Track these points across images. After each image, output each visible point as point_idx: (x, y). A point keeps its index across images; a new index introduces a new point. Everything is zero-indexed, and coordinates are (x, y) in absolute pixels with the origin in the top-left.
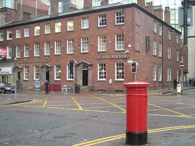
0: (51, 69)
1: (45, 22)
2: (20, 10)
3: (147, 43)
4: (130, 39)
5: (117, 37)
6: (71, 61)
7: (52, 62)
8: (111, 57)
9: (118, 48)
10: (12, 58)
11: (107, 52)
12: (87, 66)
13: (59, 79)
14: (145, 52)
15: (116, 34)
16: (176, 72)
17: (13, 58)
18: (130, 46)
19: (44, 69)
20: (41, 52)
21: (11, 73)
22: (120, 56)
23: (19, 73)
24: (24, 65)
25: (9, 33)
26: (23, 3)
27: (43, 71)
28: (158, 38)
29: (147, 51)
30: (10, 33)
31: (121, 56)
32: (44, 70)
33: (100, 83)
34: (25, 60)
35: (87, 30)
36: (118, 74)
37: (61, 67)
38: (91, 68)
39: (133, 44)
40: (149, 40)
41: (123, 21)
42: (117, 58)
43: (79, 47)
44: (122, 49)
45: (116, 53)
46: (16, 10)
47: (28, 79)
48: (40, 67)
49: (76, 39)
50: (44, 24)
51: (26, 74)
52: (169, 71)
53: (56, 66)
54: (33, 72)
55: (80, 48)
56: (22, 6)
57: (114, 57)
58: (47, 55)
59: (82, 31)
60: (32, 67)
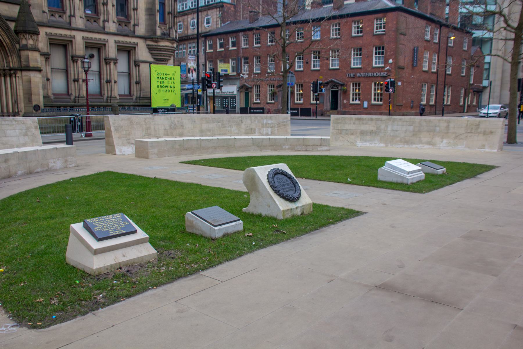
4: (392, 53)
5: (376, 49)
14: (410, 67)
16: (459, 92)
21: (235, 93)
22: (378, 74)
30: (232, 40)
31: (380, 74)
33: (353, 106)
36: (375, 95)
43: (327, 61)
45: (373, 70)
48: (275, 86)
52: (448, 91)
54: (267, 93)
55: (328, 62)
60: (265, 85)
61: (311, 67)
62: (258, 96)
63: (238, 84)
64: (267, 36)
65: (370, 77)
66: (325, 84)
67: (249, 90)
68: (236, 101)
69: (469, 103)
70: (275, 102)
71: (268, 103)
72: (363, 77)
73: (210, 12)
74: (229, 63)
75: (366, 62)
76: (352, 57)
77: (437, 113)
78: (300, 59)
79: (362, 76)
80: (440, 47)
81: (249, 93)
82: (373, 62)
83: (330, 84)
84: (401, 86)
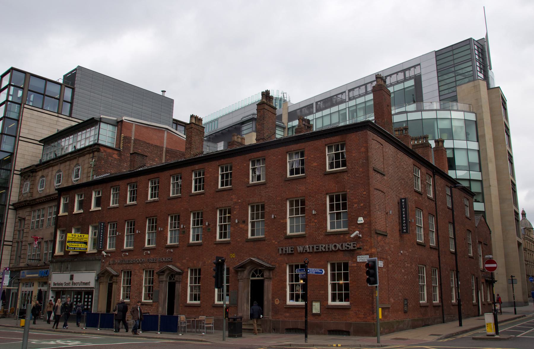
0: (181, 276)
1: (172, 172)
3: (402, 214)
4: (362, 205)
5: (331, 200)
6: (218, 258)
7: (184, 261)
8: (317, 249)
11: (307, 235)
13: (198, 302)
14: (397, 234)
15: (327, 194)
19: (164, 278)
20: (161, 237)
21: (92, 285)
23: (110, 286)
25: (96, 195)
27: (162, 281)
28: (427, 204)
29: (403, 232)
31: (342, 245)
32: (164, 279)
34: (126, 255)
35: (262, 187)
36: (334, 289)
37: (202, 273)
38: (270, 275)
40: (405, 207)
41: (344, 164)
42: (331, 250)
43: (243, 226)
47: (129, 301)
48: (155, 272)
49: (236, 207)
53: (192, 270)
54: (141, 285)
57: (325, 248)
61: (216, 237)
62: (127, 289)
63: (98, 268)
64: (148, 187)
65: (322, 251)
66: (239, 268)
67: (114, 278)
68: (92, 298)
69: (483, 300)
70: (153, 302)
71: (143, 304)
72: (309, 253)
73: (81, 159)
74: (88, 234)
75: (314, 224)
76: (288, 216)
77: (445, 319)
78: (198, 225)
79: (308, 251)
80: (437, 207)
81: (114, 285)
82: (326, 223)
83: (248, 268)
84: (384, 270)
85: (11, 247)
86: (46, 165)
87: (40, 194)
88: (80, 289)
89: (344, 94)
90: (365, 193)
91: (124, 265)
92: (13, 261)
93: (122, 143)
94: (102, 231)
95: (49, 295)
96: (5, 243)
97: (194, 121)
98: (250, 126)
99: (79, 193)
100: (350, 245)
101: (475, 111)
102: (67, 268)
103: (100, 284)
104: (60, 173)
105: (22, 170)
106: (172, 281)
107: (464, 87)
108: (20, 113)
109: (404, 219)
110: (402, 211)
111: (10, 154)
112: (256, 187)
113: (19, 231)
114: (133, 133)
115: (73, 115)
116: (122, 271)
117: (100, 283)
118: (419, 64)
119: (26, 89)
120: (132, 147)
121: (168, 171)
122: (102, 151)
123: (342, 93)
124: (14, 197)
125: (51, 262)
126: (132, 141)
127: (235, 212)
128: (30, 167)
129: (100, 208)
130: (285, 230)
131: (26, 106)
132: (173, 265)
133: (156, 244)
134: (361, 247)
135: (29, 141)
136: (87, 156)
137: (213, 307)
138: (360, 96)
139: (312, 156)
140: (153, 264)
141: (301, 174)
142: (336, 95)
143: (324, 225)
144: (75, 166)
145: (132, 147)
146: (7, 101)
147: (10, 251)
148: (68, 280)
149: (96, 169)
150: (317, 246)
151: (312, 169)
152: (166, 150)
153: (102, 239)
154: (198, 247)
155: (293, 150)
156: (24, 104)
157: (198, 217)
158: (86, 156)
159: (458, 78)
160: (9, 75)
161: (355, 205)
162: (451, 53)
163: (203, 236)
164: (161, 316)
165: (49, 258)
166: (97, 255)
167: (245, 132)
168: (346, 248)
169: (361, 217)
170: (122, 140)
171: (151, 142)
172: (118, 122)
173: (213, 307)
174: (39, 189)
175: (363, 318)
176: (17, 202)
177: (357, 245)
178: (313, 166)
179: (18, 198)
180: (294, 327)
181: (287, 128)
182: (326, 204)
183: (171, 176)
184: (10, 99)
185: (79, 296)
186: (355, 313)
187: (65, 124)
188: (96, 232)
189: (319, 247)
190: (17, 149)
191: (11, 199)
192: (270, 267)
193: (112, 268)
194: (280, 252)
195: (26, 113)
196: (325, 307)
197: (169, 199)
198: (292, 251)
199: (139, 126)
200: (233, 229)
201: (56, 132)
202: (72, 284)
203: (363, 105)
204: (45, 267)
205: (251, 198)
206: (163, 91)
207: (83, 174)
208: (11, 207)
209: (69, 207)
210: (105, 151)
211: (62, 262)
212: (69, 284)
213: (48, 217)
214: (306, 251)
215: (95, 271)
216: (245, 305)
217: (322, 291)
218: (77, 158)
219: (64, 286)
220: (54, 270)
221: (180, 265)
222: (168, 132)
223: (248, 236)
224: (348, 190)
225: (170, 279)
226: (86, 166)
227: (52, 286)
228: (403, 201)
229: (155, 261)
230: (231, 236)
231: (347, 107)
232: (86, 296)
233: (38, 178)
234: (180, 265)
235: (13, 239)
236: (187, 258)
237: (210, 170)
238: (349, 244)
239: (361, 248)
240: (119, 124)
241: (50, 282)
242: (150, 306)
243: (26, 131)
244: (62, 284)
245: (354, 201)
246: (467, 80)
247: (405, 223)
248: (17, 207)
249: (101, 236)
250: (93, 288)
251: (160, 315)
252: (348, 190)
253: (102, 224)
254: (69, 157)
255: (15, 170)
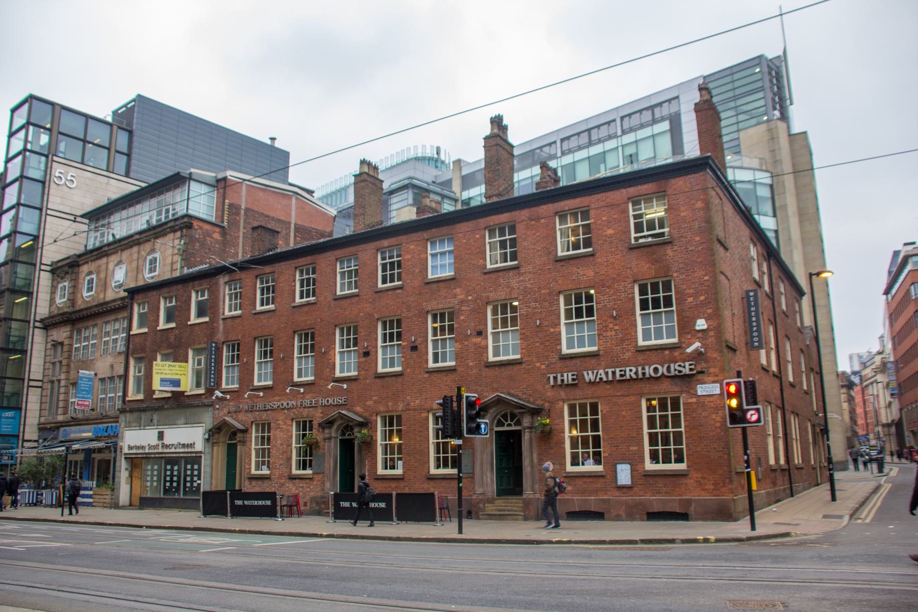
1: (338, 253)
2: (238, 227)
3: (750, 317)
4: (702, 298)
5: (643, 291)
7: (369, 403)
9: (570, 345)
10: (206, 389)
11: (601, 352)
12: (513, 416)
15: (635, 281)
17: (210, 391)
18: (701, 324)
19: (333, 432)
21: (199, 447)
24: (250, 417)
25: (197, 297)
26: (246, 204)
31: (668, 369)
33: (579, 482)
39: (715, 316)
42: (647, 376)
44: (587, 349)
45: (640, 358)
46: (223, 227)
48: (315, 424)
49: (463, 308)
50: (333, 258)
51: (262, 453)
54: (290, 445)
56: (246, 214)
58: (346, 374)
59: (491, 275)
60: (285, 423)
63: (208, 419)
65: (631, 379)
67: (239, 435)
68: (199, 470)
70: (314, 474)
71: (293, 478)
72: (606, 382)
74: (187, 362)
75: (614, 333)
78: (348, 346)
79: (605, 379)
83: (491, 411)
85: (40, 389)
86: (96, 253)
87: (88, 302)
88: (178, 455)
89: (553, 146)
90: (706, 278)
91: (257, 413)
92: (46, 413)
93: (226, 215)
94: (213, 357)
95: (121, 467)
96: (32, 383)
97: (366, 169)
98: (405, 196)
99: (197, 289)
100: (684, 367)
101: (770, 168)
102: (152, 420)
103: (213, 446)
104: (155, 255)
105: (53, 264)
106: (346, 437)
107: (751, 131)
108: (48, 170)
109: (754, 324)
110: (750, 312)
111: (32, 238)
112: (500, 274)
113: (54, 364)
114: (244, 199)
115: (132, 174)
116: (252, 422)
117: (213, 443)
118: (677, 97)
119: (55, 132)
120: (242, 221)
121: (333, 252)
122: (196, 227)
123: (550, 144)
124: (42, 309)
125: (123, 411)
126: (242, 212)
127: (462, 318)
128: (68, 258)
129: (207, 319)
130: (558, 345)
131: (55, 158)
132: (348, 410)
133: (315, 375)
134: (704, 370)
135: (62, 215)
136: (171, 235)
137: (428, 479)
138: (580, 148)
139: (604, 218)
140: (311, 409)
141: (584, 248)
142: (541, 148)
143: (633, 334)
144: (149, 254)
145: (242, 221)
146: (25, 150)
147: (40, 397)
148: (154, 441)
149: (187, 256)
150: (621, 371)
151: (606, 241)
152: (295, 227)
153: (214, 371)
154: (394, 378)
155: (567, 208)
156: (53, 155)
157: (349, 334)
158: (168, 235)
159: (741, 117)
160: (26, 106)
161: (690, 299)
162: (729, 79)
163: (403, 359)
164: (397, 495)
165: (119, 404)
166: (206, 398)
167: (394, 207)
168: (677, 373)
169: (701, 318)
170: (226, 209)
171: (271, 214)
172: (218, 181)
173: (428, 479)
174: (85, 294)
175: (713, 490)
176: (47, 316)
177: (695, 366)
178: (606, 236)
179: (48, 309)
180: (583, 509)
181: (460, 201)
182: (633, 298)
183: (337, 259)
184: (29, 147)
185: (176, 468)
186: (697, 481)
187: (118, 188)
188: (201, 359)
189: (625, 371)
190: (44, 228)
191: (38, 311)
192: (534, 409)
193: (235, 419)
194: (552, 383)
195: (57, 170)
196: (640, 473)
197: (335, 300)
198: (573, 380)
199: (253, 189)
200: (460, 346)
201: (106, 202)
202: (163, 447)
203: (529, 181)
204: (104, 420)
205: (491, 292)
206: (273, 139)
207: (164, 265)
208: (37, 324)
209: (149, 319)
210: (201, 228)
211: (144, 410)
212: (156, 447)
213: (104, 339)
214: (601, 379)
215: (204, 425)
216: (489, 474)
217: (634, 446)
218: (153, 240)
219: (147, 451)
220: (129, 426)
221: (361, 410)
222: (297, 198)
223: (487, 358)
224: (675, 275)
225: (343, 434)
226: (170, 251)
227: (126, 450)
228: (752, 294)
229: (313, 405)
230: (456, 359)
231: (620, 144)
232: (169, 467)
233: (82, 275)
234: (361, 410)
235: (44, 376)
236: (374, 398)
237: (411, 247)
238: (683, 365)
239: (702, 372)
240: (221, 185)
241: (121, 444)
242: (308, 481)
243: (58, 200)
244: (143, 447)
245: (688, 291)
246: (754, 121)
247: (756, 331)
248: (48, 325)
249: (213, 364)
250: (201, 452)
251: (394, 493)
252: (675, 275)
253: (214, 345)
254: (137, 239)
255: (41, 264)
